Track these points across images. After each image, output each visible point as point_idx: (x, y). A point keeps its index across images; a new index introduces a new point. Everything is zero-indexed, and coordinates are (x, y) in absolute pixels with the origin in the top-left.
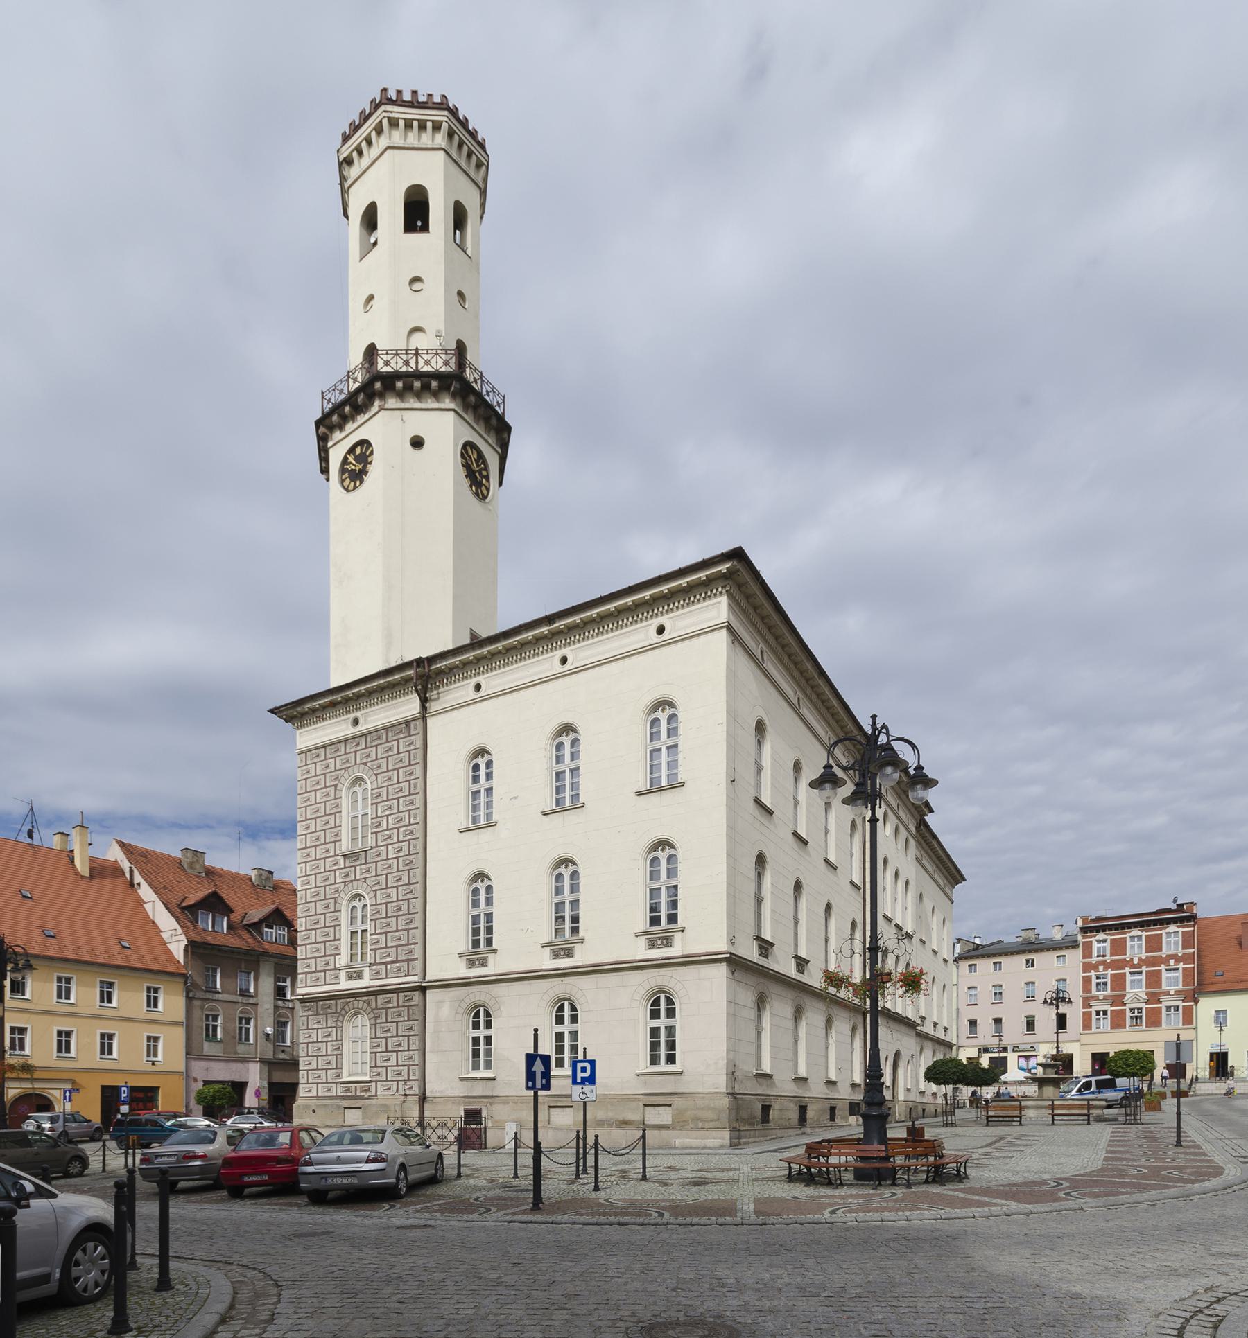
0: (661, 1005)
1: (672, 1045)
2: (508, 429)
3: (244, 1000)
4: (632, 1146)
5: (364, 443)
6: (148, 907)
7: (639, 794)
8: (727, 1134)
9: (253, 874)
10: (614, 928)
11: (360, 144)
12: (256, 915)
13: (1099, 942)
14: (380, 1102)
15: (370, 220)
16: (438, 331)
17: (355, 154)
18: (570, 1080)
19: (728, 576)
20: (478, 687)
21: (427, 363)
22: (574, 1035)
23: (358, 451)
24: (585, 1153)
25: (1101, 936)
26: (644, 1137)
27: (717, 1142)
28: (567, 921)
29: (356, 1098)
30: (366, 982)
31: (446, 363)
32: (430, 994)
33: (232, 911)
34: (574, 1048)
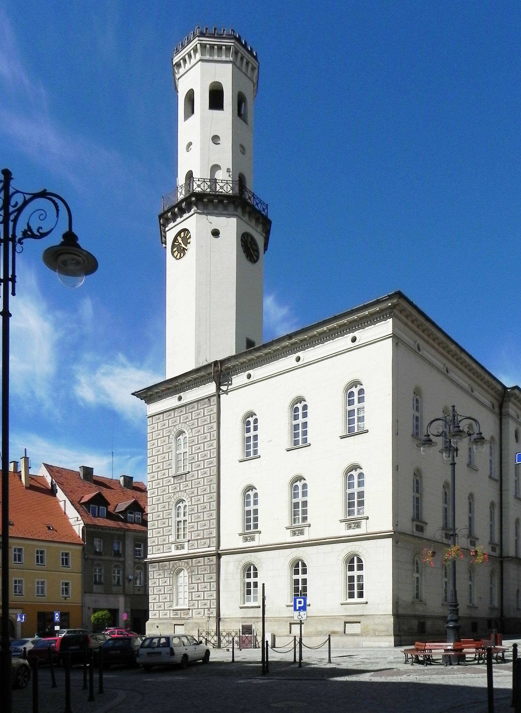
0: (353, 562)
1: (361, 587)
2: (270, 222)
3: (116, 559)
5: (185, 230)
6: (62, 504)
7: (342, 437)
8: (392, 639)
9: (122, 480)
10: (326, 516)
11: (185, 56)
12: (122, 506)
14: (194, 621)
15: (190, 97)
16: (228, 169)
17: (182, 61)
18: (293, 608)
19: (394, 306)
20: (249, 376)
21: (222, 187)
26: (329, 639)
27: (387, 644)
29: (181, 619)
30: (185, 551)
31: (232, 189)
32: (223, 559)
33: (109, 504)
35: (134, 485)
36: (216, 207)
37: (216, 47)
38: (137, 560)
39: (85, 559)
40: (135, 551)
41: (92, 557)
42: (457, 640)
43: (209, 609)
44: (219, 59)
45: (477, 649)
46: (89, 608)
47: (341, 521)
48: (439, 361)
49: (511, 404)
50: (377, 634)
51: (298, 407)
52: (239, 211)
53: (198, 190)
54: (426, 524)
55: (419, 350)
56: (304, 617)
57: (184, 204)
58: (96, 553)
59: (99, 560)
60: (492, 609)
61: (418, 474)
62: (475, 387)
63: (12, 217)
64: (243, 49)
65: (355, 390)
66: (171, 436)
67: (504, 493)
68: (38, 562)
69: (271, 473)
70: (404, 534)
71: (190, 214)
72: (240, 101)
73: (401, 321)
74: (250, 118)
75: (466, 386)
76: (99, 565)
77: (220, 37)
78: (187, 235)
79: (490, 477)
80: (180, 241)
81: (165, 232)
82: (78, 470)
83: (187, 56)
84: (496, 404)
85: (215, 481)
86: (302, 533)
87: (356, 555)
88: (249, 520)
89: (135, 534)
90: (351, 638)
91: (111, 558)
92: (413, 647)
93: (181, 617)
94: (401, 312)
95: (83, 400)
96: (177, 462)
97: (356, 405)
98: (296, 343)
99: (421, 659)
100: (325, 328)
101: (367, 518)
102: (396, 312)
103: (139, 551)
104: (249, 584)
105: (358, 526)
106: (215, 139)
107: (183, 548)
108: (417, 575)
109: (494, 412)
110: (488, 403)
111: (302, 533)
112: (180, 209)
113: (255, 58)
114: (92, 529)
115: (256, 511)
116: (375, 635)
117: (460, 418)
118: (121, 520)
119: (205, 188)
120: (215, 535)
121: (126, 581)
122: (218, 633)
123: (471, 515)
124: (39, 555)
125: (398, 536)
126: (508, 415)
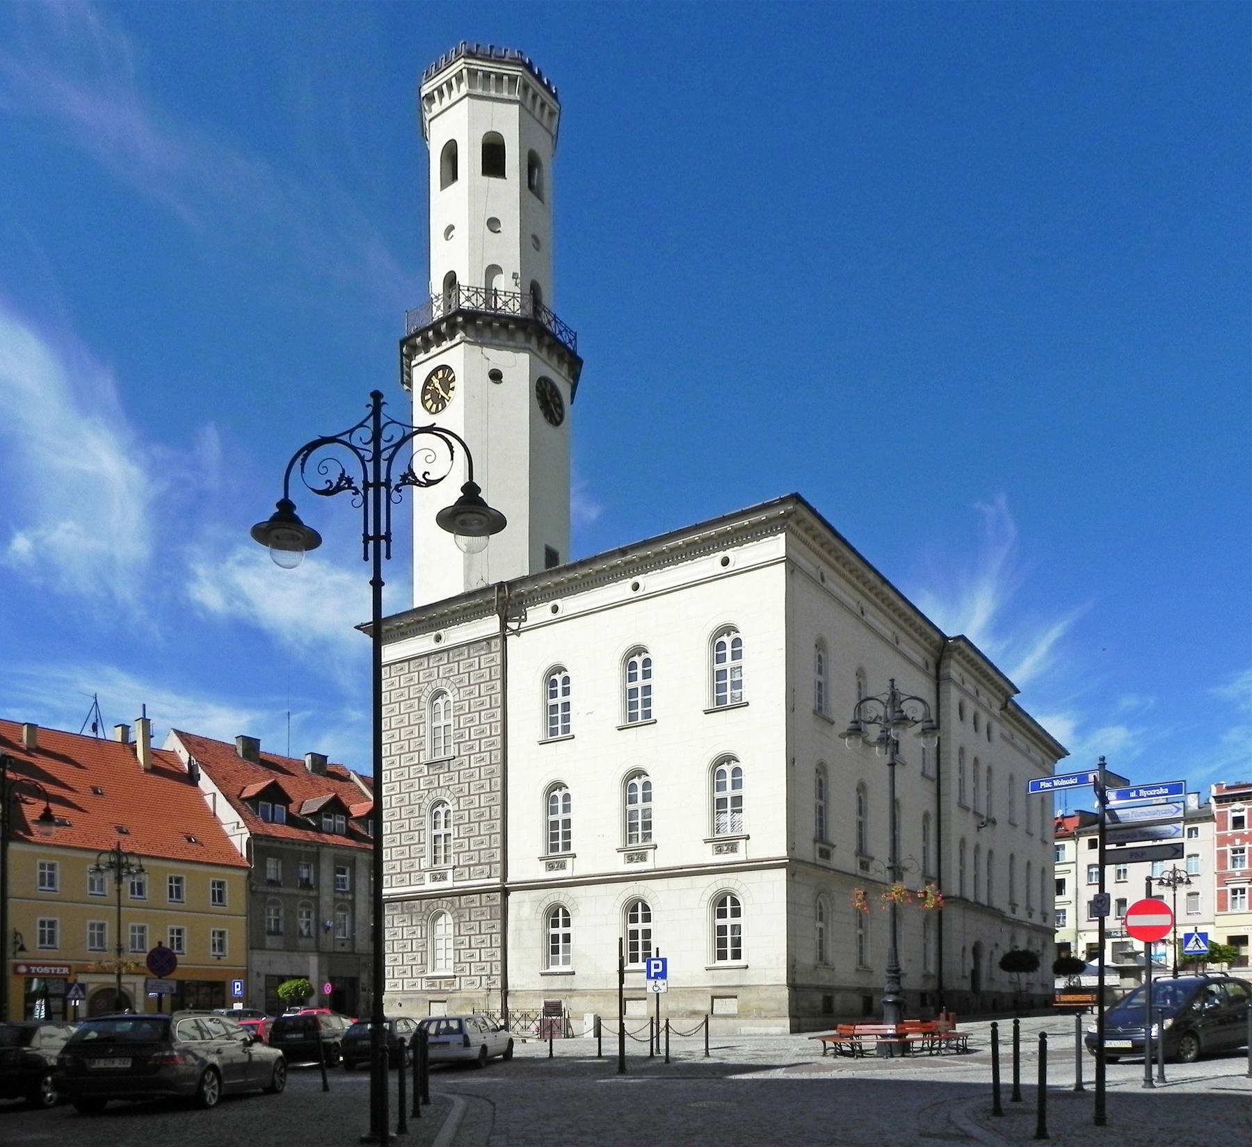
0: (725, 905)
1: (737, 942)
3: (304, 893)
4: (697, 1029)
5: (444, 367)
6: (209, 800)
8: (787, 1022)
9: (308, 759)
10: (681, 832)
12: (313, 805)
13: (1234, 811)
14: (464, 995)
15: (451, 152)
19: (788, 515)
22: (647, 933)
23: (440, 374)
24: (658, 1033)
25: (1238, 805)
26: (707, 1021)
27: (778, 1030)
28: (637, 829)
29: (441, 992)
30: (448, 884)
32: (513, 897)
34: (647, 946)
35: (329, 769)
36: (495, 334)
37: (493, 76)
38: (339, 895)
39: (252, 892)
40: (336, 880)
41: (262, 888)
42: (899, 1022)
43: (489, 977)
44: (498, 95)
45: (925, 1034)
46: (258, 974)
47: (706, 841)
48: (887, 629)
49: (952, 663)
50: (763, 1014)
51: (636, 662)
52: (534, 343)
53: (466, 305)
54: (834, 846)
55: (823, 580)
56: (663, 989)
57: (443, 327)
58: (272, 883)
59: (276, 894)
60: (926, 976)
61: (821, 770)
62: (902, 635)
63: (385, 455)
64: (534, 81)
65: (727, 640)
66: (423, 699)
67: (943, 799)
68: (171, 896)
69: (592, 763)
70: (803, 862)
71: (454, 342)
72: (532, 164)
73: (798, 537)
74: (548, 192)
75: (888, 634)
76: (274, 903)
77: (500, 60)
78: (449, 375)
79: (923, 774)
80: (437, 385)
81: (410, 367)
82: (234, 742)
83: (444, 87)
84: (931, 661)
85: (499, 772)
86: (643, 858)
87: (731, 894)
88: (554, 837)
89: (336, 851)
90: (722, 1021)
91: (296, 891)
92: (834, 1032)
93: (440, 989)
94: (798, 523)
95: (203, 608)
96: (434, 740)
97: (729, 663)
98: (632, 561)
99: (844, 1048)
100: (680, 542)
101: (748, 838)
102: (792, 523)
103: (343, 880)
104: (555, 938)
105: (733, 849)
106: (493, 224)
107: (444, 878)
108: (819, 925)
109: (928, 675)
110: (918, 660)
111: (643, 858)
112: (438, 333)
113: (555, 96)
114: (263, 843)
115: (567, 823)
116: (759, 1016)
117: (903, 698)
118: (308, 827)
119: (479, 303)
120: (498, 859)
121: (322, 930)
122: (505, 1013)
123: (861, 818)
124: (47, 871)
125: (794, 866)
126: (949, 679)
